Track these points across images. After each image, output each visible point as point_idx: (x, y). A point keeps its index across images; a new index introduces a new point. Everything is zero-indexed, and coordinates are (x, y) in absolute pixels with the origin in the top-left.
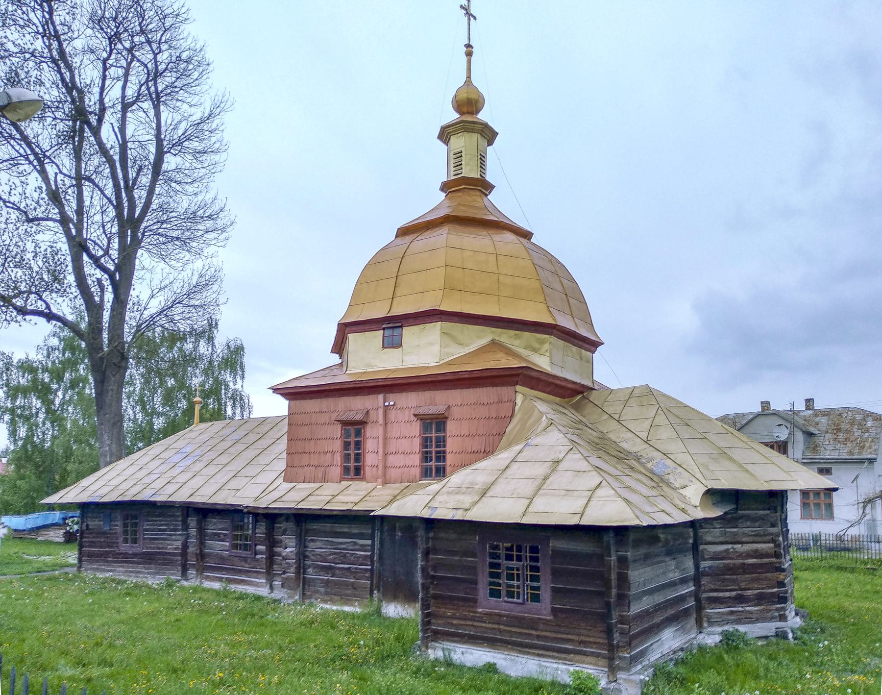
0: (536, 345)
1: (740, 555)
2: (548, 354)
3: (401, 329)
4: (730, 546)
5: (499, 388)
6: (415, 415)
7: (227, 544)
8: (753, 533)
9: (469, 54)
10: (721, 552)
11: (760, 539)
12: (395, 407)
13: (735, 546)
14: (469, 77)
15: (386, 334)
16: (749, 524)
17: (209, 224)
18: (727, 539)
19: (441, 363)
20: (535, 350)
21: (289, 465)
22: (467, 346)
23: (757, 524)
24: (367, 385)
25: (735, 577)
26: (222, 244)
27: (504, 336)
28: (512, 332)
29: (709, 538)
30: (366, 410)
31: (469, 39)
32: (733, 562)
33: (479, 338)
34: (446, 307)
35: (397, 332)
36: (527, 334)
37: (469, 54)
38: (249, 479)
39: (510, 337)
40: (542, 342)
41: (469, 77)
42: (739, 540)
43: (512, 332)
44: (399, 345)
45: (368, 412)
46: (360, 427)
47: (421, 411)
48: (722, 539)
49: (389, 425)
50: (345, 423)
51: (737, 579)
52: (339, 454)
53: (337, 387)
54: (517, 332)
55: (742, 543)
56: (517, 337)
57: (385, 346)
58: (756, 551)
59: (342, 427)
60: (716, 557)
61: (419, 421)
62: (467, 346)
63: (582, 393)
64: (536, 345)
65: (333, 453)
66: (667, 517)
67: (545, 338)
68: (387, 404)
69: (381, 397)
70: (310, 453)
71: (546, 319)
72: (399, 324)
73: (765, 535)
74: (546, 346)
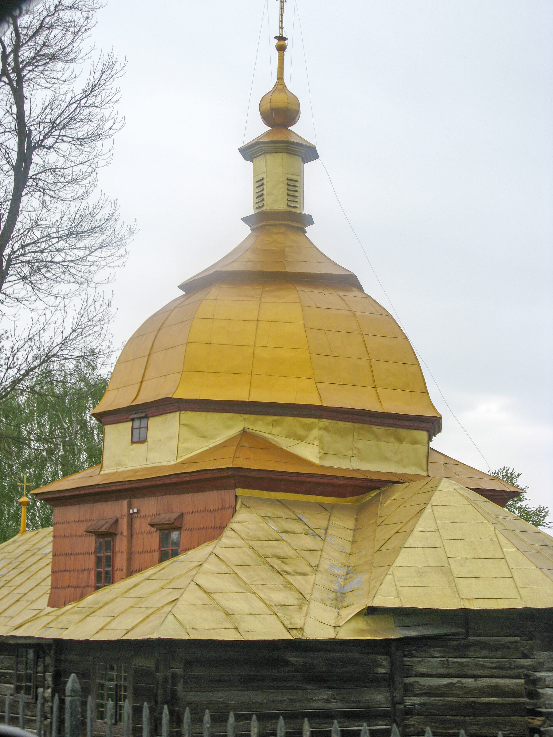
0: (302, 432)
1: (470, 692)
2: (317, 442)
3: (146, 420)
4: (455, 680)
5: (223, 492)
6: (152, 525)
7: (12, 686)
8: (493, 665)
9: (281, 49)
10: (440, 686)
11: (502, 673)
12: (139, 515)
13: (464, 680)
14: (281, 77)
15: (135, 426)
16: (485, 653)
17: (97, 239)
18: (451, 671)
19: (178, 461)
20: (301, 439)
21: (54, 586)
22: (212, 438)
23: (498, 654)
24: (110, 489)
25: (462, 718)
26: (120, 262)
27: (260, 423)
28: (270, 418)
29: (422, 669)
30: (115, 519)
31: (282, 28)
32: (456, 699)
33: (228, 427)
34: (180, 394)
35: (144, 422)
36: (289, 420)
37: (281, 49)
38: (29, 603)
39: (268, 424)
40: (309, 428)
41: (281, 77)
42: (470, 672)
43: (270, 418)
44: (143, 441)
45: (117, 521)
46: (110, 539)
47: (156, 520)
48: (443, 671)
49: (135, 536)
50: (99, 535)
51: (465, 722)
52: (93, 571)
53: (86, 492)
54: (275, 418)
55: (476, 677)
56: (274, 424)
57: (134, 440)
58: (496, 687)
59: (96, 539)
60: (431, 692)
61: (158, 531)
62: (213, 439)
63: (378, 488)
64: (302, 432)
65: (89, 570)
66: (152, 609)
67: (313, 423)
68: (131, 511)
69: (125, 503)
70: (70, 571)
71: (312, 400)
72: (143, 415)
73: (512, 668)
74: (315, 432)
